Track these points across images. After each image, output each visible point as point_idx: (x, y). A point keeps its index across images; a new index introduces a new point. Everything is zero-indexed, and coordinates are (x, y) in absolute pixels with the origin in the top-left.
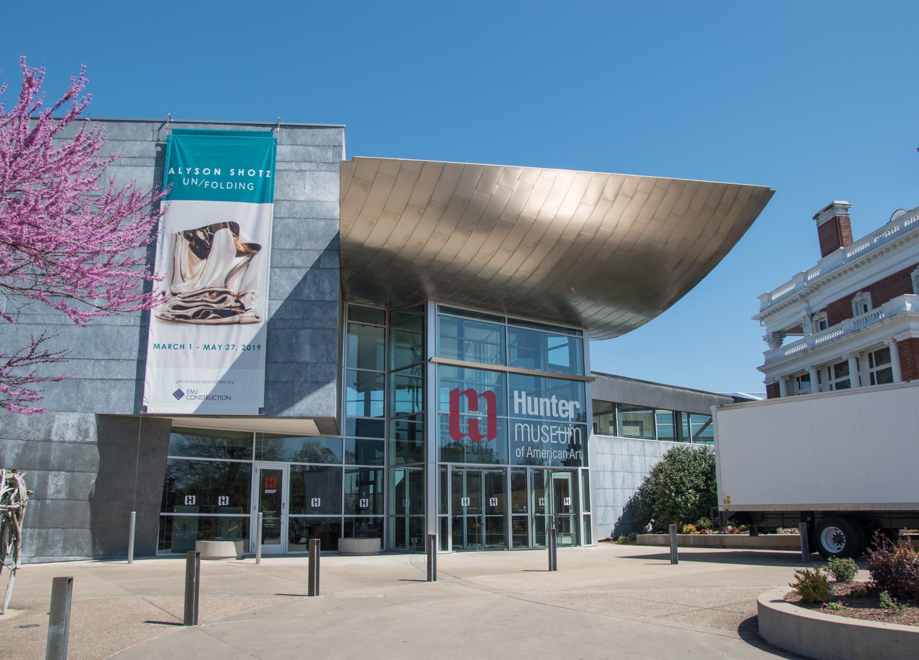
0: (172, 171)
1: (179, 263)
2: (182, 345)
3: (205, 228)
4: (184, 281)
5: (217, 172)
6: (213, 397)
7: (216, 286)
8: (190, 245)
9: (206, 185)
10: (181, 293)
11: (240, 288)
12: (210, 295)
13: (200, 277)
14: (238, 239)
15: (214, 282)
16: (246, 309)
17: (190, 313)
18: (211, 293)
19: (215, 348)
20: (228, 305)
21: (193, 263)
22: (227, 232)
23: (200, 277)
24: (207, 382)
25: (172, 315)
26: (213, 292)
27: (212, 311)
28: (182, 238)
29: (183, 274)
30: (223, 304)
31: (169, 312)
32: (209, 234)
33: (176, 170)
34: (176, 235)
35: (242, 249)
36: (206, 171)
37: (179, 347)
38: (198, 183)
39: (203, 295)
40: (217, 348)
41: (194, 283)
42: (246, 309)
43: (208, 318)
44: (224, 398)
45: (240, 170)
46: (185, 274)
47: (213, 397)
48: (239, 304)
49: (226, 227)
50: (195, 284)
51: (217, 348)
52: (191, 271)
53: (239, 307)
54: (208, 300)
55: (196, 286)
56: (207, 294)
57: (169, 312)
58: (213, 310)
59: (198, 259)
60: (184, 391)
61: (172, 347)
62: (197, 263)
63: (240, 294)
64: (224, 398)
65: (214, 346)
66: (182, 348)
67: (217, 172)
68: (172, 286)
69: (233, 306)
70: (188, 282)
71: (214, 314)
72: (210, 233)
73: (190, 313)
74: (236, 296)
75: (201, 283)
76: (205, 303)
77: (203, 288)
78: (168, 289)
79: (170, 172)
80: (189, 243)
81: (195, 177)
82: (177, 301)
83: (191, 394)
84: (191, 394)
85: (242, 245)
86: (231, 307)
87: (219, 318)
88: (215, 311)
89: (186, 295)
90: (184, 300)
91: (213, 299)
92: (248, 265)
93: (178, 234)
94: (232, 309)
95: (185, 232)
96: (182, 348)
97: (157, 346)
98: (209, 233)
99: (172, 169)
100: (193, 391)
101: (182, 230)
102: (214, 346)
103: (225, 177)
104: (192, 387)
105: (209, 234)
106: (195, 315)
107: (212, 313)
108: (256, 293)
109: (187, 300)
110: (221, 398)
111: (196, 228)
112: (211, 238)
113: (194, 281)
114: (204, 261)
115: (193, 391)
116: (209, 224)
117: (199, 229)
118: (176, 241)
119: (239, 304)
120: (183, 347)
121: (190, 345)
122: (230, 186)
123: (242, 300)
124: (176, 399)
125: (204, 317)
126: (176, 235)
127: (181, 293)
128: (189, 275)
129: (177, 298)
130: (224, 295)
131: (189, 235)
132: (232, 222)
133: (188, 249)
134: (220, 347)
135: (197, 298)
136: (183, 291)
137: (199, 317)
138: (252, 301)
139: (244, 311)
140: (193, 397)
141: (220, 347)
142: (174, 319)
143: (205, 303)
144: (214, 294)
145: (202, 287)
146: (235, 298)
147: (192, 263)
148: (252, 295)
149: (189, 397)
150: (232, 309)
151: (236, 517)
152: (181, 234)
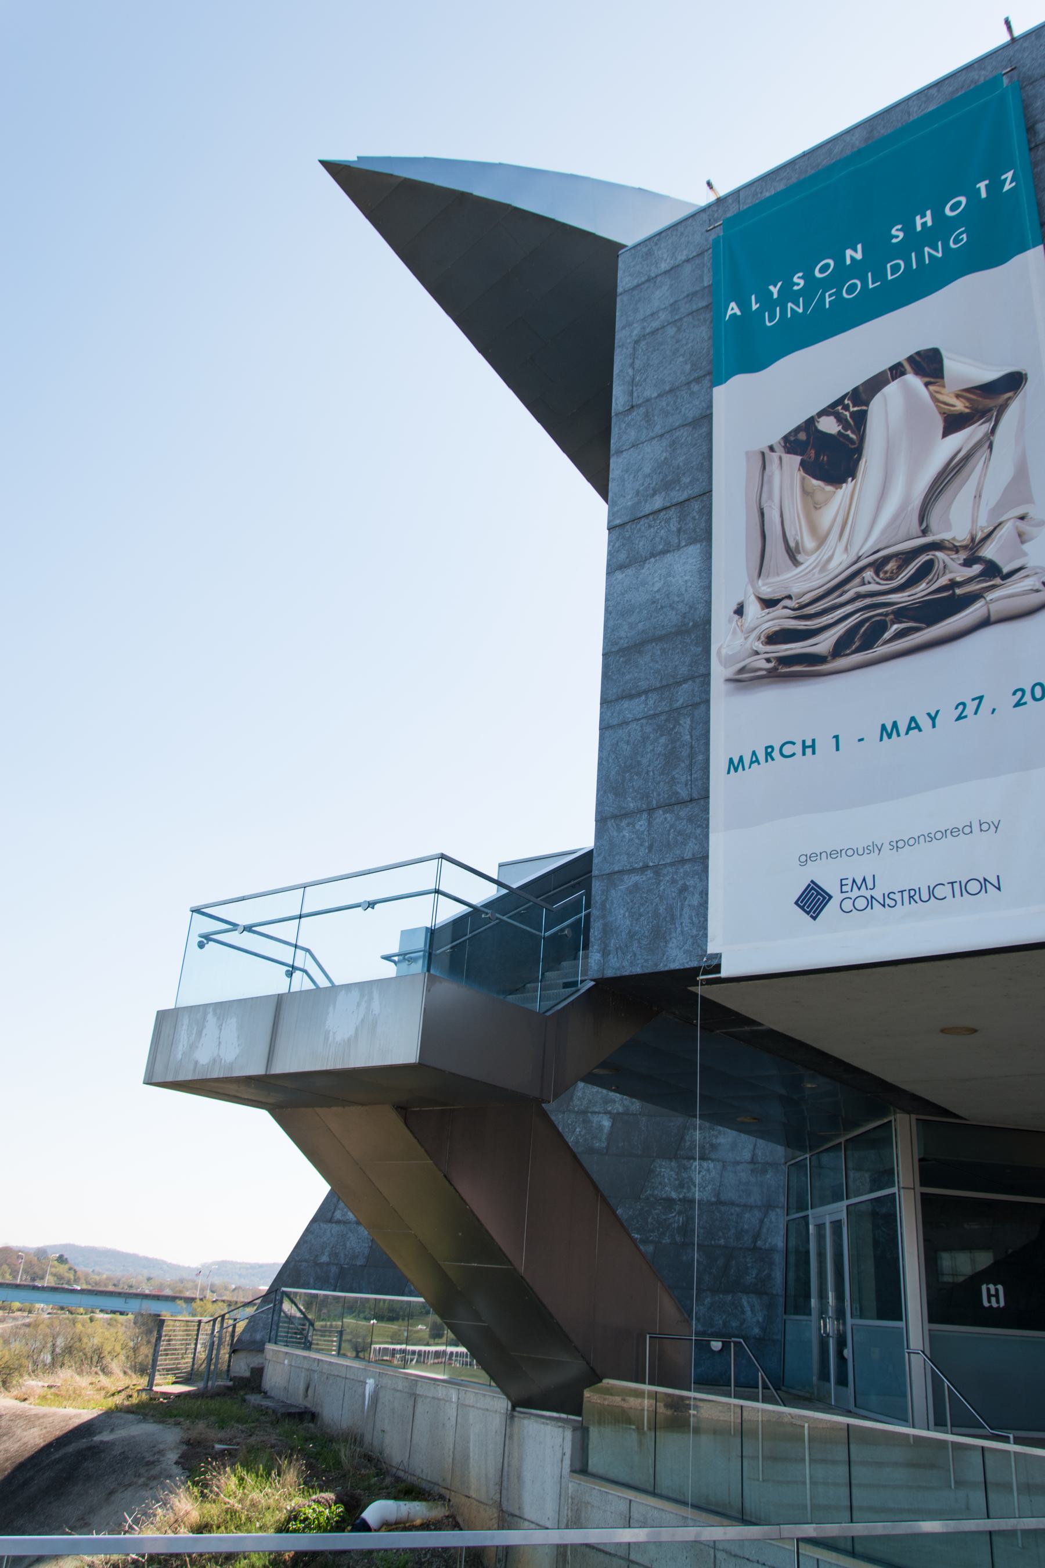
0: (734, 309)
1: (778, 520)
2: (809, 743)
3: (840, 401)
4: (796, 563)
5: (854, 254)
6: (931, 892)
7: (892, 541)
8: (803, 464)
9: (828, 300)
10: (789, 597)
11: (974, 521)
12: (878, 575)
13: (909, 596)
14: (944, 386)
15: (885, 531)
16: (1006, 570)
17: (823, 644)
18: (878, 566)
19: (918, 727)
20: (943, 581)
21: (817, 507)
22: (908, 391)
23: (909, 596)
24: (906, 843)
25: (768, 660)
26: (887, 559)
27: (891, 617)
28: (780, 459)
29: (792, 544)
30: (923, 585)
31: (757, 653)
32: (852, 414)
33: (744, 305)
34: (763, 454)
35: (960, 406)
36: (824, 268)
37: (798, 748)
38: (805, 309)
39: (857, 580)
40: (924, 722)
41: (826, 557)
42: (1006, 570)
43: (880, 642)
44: (974, 887)
45: (930, 224)
46: (797, 544)
47: (931, 892)
48: (977, 568)
49: (903, 373)
50: (830, 559)
51: (924, 722)
52: (813, 529)
53: (982, 574)
54: (873, 587)
55: (833, 564)
56: (869, 574)
57: (757, 653)
58: (893, 612)
59: (829, 488)
60: (830, 886)
61: (776, 754)
62: (827, 501)
63: (979, 536)
64: (974, 887)
65: (913, 719)
66: (809, 751)
67: (854, 254)
68: (760, 582)
69: (959, 579)
70: (808, 562)
71: (901, 622)
72: (856, 409)
73: (823, 644)
74: (965, 547)
75: (846, 549)
76: (868, 601)
77: (856, 558)
78: (750, 590)
79: (730, 312)
80: (798, 459)
81: (794, 297)
82: (780, 619)
83: (856, 893)
84: (853, 895)
85: (958, 396)
86: (953, 584)
87: (917, 630)
88: (901, 614)
89: (807, 598)
90: (801, 612)
91: (891, 579)
92: (991, 447)
93: (767, 451)
94: (958, 591)
95: (786, 438)
96: (809, 751)
97: (734, 765)
98: (852, 409)
99: (733, 305)
100: (859, 882)
101: (776, 437)
102: (913, 719)
103: (873, 263)
104: (857, 868)
105: (852, 414)
106: (840, 648)
107: (893, 623)
108: (1032, 514)
109: (812, 612)
110: (964, 889)
111: (813, 412)
112: (860, 420)
113: (825, 553)
114: (848, 487)
115: (859, 882)
116: (849, 388)
117: (823, 413)
118: (764, 468)
119: (977, 568)
120: (813, 746)
121: (836, 737)
122: (895, 269)
123: (989, 552)
124: (808, 917)
125: (867, 644)
126: (763, 454)
127: (789, 597)
128: (809, 543)
129: (778, 611)
130: (924, 558)
131: (797, 441)
132: (918, 353)
133: (798, 475)
134: (933, 719)
135: (841, 595)
136: (795, 589)
137: (854, 647)
138: (1023, 542)
139: (998, 581)
140: (861, 903)
141: (933, 719)
142: (775, 669)
143: (868, 601)
144: (891, 566)
145: (852, 557)
146: (963, 556)
147: (812, 504)
148: (1019, 523)
149: (848, 905)
150: (958, 591)
151: (985, 1191)
152: (776, 448)
